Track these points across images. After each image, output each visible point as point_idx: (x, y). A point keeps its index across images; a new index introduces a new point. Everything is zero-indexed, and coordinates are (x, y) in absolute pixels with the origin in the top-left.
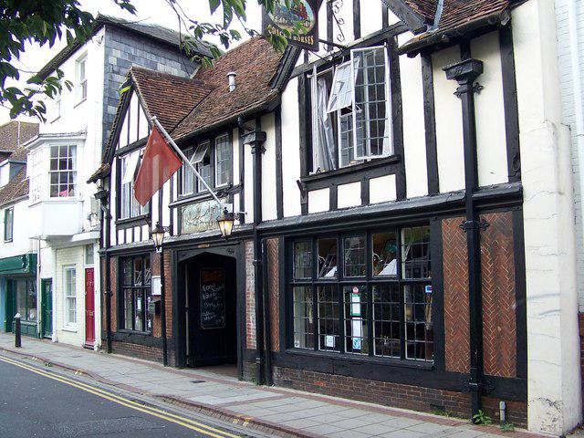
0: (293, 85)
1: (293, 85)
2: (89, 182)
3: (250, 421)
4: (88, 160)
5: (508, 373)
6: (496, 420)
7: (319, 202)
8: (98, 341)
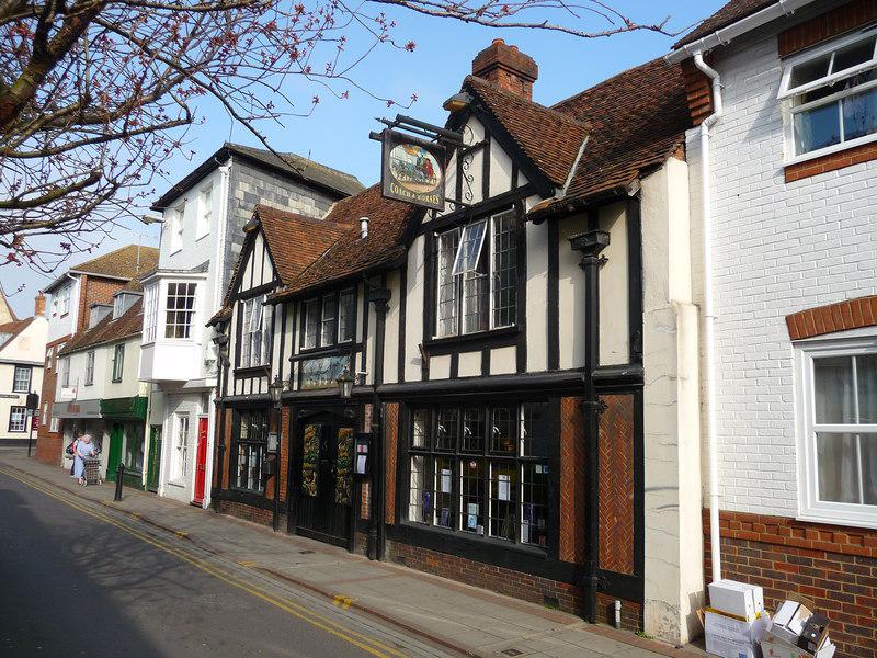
0: (420, 242)
1: (420, 242)
2: (207, 326)
3: (352, 605)
4: (209, 300)
5: (626, 569)
6: (612, 622)
7: (440, 368)
8: (207, 500)
